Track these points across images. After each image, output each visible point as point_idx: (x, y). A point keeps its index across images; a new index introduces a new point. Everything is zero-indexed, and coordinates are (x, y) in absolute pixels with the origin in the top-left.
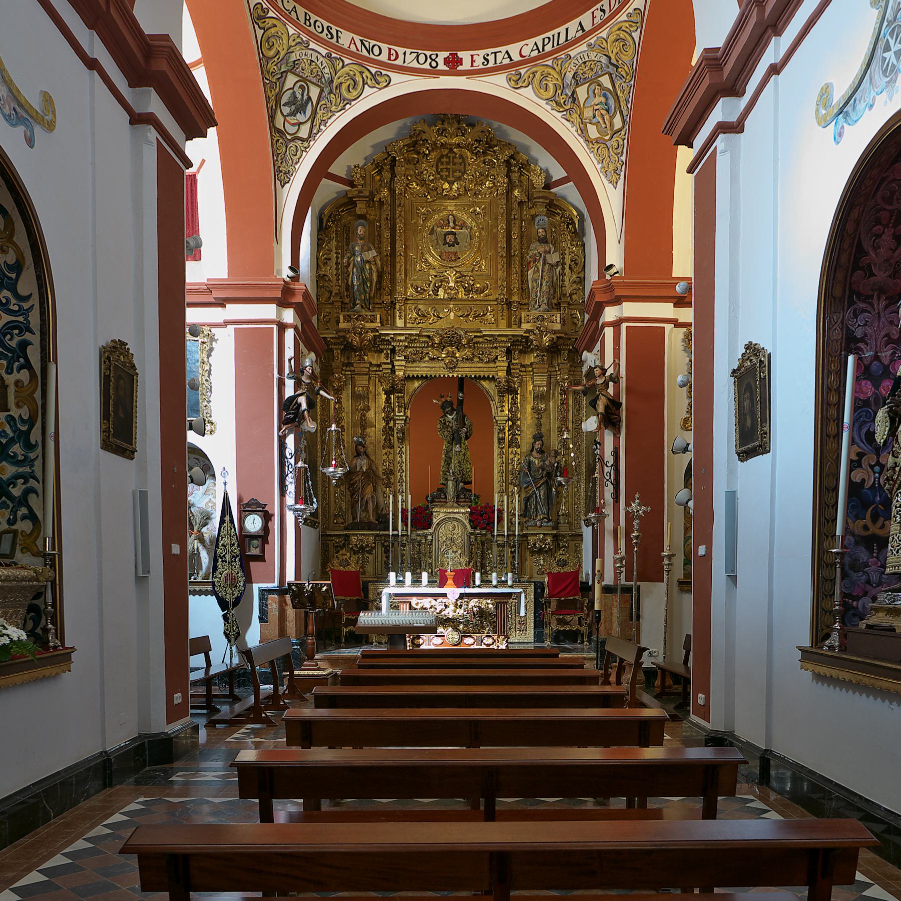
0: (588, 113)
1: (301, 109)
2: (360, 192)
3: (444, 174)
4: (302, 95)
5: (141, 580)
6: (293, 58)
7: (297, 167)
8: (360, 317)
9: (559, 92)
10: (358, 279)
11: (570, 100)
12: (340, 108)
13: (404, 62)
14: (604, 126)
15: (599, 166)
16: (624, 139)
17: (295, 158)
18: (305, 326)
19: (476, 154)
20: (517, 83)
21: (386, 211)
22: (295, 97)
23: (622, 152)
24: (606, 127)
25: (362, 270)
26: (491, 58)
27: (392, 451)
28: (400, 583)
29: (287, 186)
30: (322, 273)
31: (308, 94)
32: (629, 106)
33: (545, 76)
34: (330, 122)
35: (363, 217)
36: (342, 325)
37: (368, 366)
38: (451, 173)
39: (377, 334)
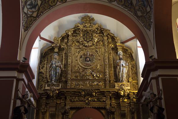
0: (137, 8)
1: (34, 7)
3: (86, 39)
7: (31, 26)
9: (126, 2)
10: (54, 72)
11: (130, 4)
12: (48, 8)
14: (143, 11)
16: (151, 14)
17: (31, 23)
18: (29, 83)
19: (96, 33)
22: (32, 3)
23: (151, 19)
24: (144, 12)
25: (55, 69)
29: (27, 31)
31: (37, 3)
32: (152, 3)
36: (47, 88)
37: (56, 103)
38: (88, 39)
39: (60, 91)
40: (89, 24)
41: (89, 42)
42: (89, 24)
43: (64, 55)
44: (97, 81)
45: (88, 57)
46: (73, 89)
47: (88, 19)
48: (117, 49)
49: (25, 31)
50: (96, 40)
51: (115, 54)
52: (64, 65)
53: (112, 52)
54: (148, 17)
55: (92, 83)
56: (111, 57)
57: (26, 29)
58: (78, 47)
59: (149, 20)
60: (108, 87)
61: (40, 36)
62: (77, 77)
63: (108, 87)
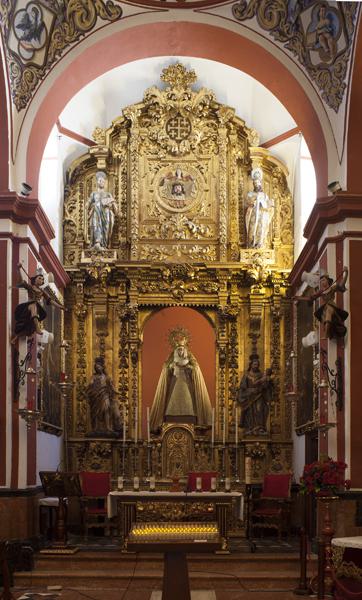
0: (311, 39)
2: (100, 149)
3: (173, 134)
4: (36, 19)
9: (283, 20)
13: (63, 131)
14: (326, 50)
15: (320, 93)
17: (31, 85)
22: (28, 20)
23: (345, 75)
25: (102, 213)
27: (126, 370)
28: (128, 485)
29: (24, 111)
30: (67, 219)
34: (64, 52)
36: (84, 260)
40: (183, 91)
41: (182, 143)
42: (183, 91)
43: (120, 177)
46: (144, 262)
47: (180, 75)
48: (251, 162)
49: (19, 111)
51: (246, 176)
52: (122, 203)
53: (236, 171)
54: (338, 68)
55: (188, 248)
56: (235, 183)
57: (23, 103)
58: (155, 156)
59: (339, 78)
61: (58, 124)
62: (152, 233)
63: (223, 259)
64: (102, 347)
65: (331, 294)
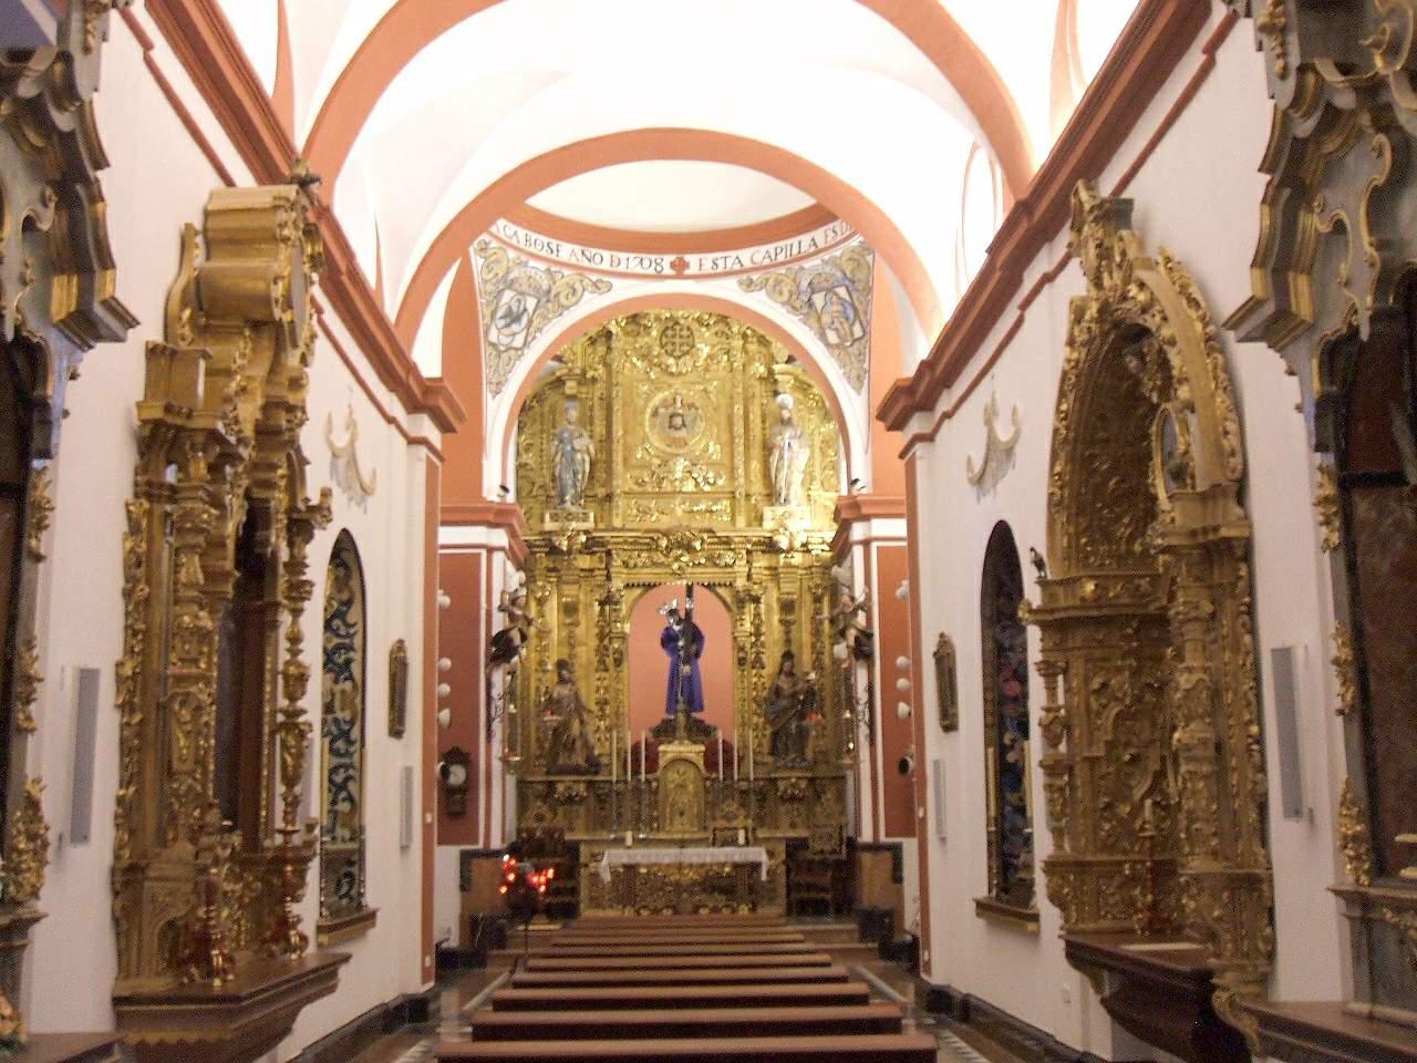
1: (516, 319)
2: (570, 370)
3: (669, 348)
5: (404, 848)
6: (512, 276)
8: (570, 517)
9: (794, 297)
20: (749, 286)
21: (599, 389)
26: (721, 263)
33: (778, 282)
35: (572, 397)
36: (549, 525)
41: (682, 359)
44: (708, 499)
45: (679, 415)
50: (706, 350)
59: (859, 361)
60: (741, 522)
63: (741, 522)
64: (571, 642)
65: (854, 613)
